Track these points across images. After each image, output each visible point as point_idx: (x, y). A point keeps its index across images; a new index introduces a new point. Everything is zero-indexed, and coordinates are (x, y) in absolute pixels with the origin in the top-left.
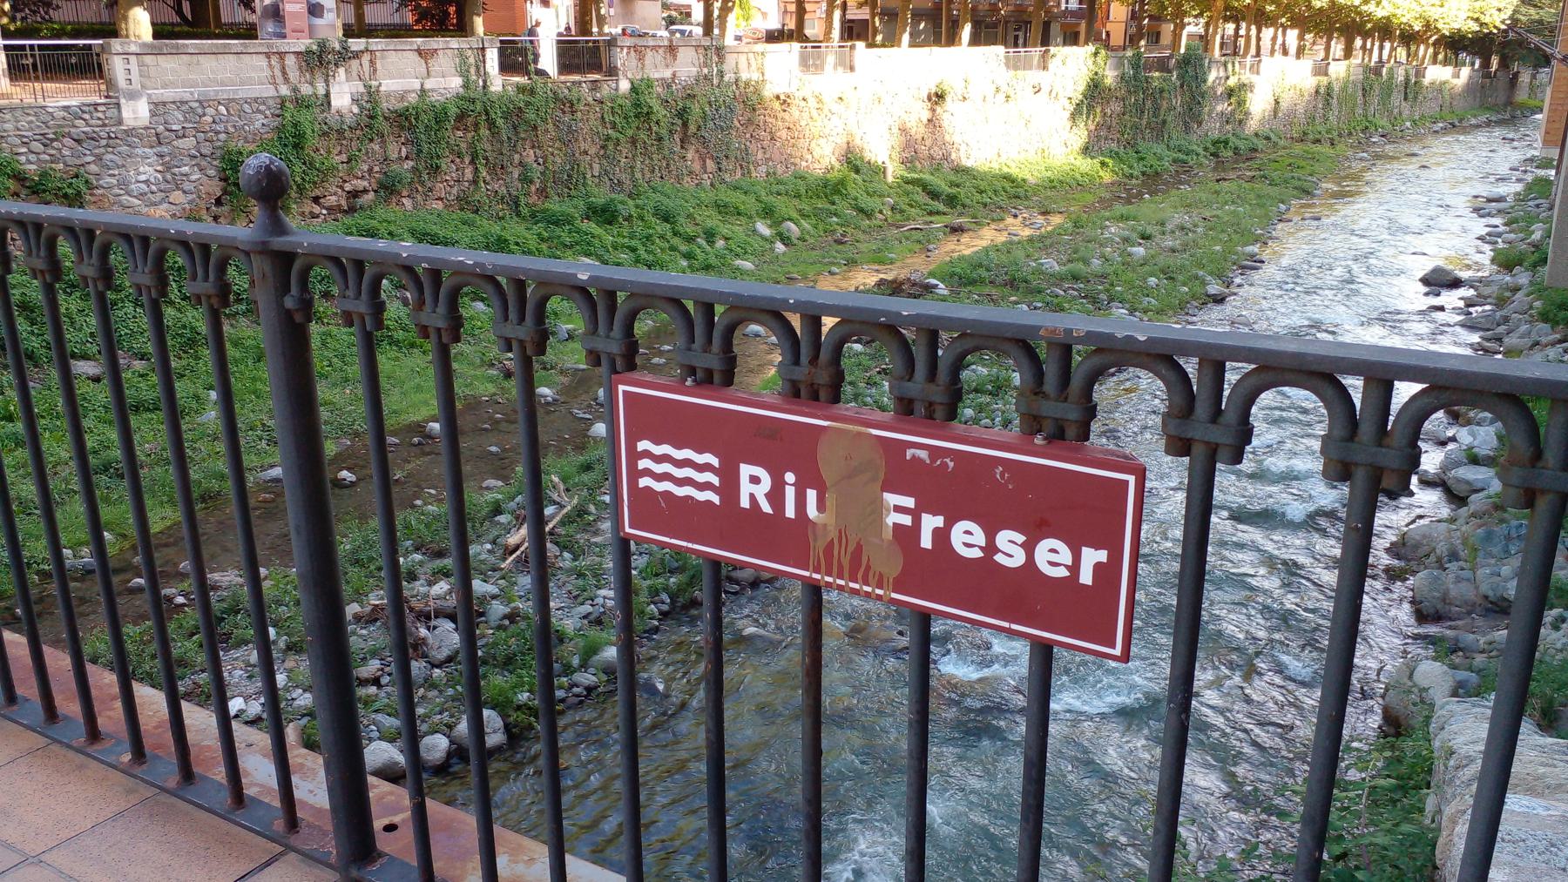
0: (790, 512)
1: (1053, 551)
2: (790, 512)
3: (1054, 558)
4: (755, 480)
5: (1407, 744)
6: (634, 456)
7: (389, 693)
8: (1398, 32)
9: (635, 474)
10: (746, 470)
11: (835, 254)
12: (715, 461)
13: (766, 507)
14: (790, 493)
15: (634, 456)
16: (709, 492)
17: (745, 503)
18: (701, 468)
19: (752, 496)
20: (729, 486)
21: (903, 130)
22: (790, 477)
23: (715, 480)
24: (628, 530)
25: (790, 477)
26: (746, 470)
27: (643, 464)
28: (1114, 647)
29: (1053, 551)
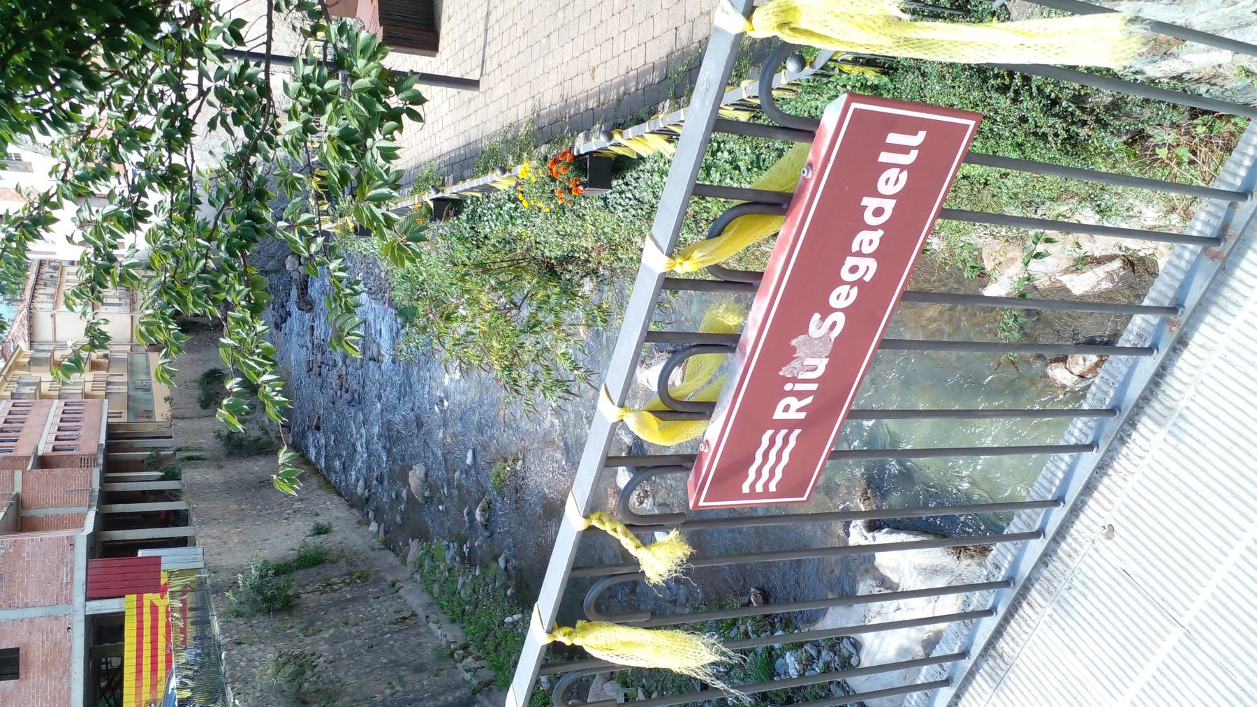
2: (814, 387)
4: (787, 408)
5: (88, 367)
7: (1175, 223)
10: (779, 414)
11: (474, 331)
12: (770, 432)
13: (809, 400)
15: (746, 497)
17: (802, 415)
18: (772, 442)
19: (799, 410)
20: (791, 425)
21: (7, 211)
23: (784, 432)
26: (779, 414)
27: (759, 489)
28: (119, 618)
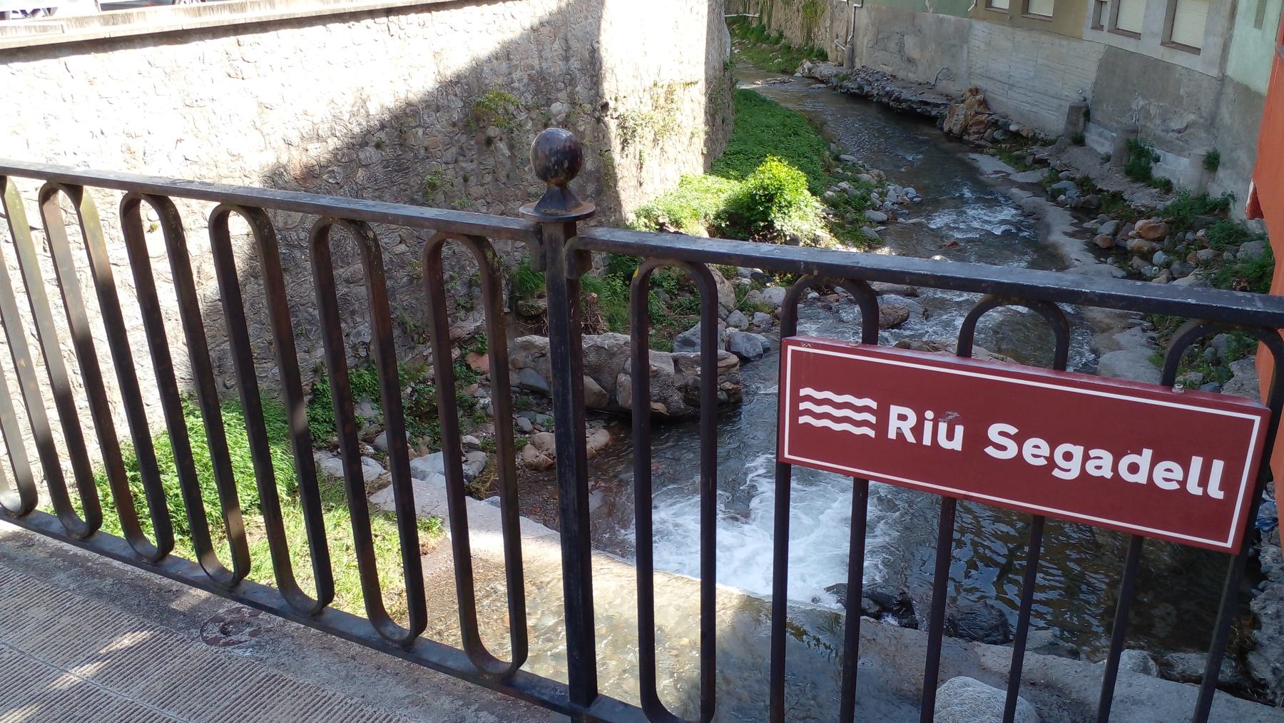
0: (927, 441)
1: (1169, 470)
2: (927, 441)
3: (1036, 451)
4: (902, 417)
6: (796, 399)
8: (273, 385)
9: (796, 413)
10: (895, 410)
12: (874, 405)
13: (910, 438)
14: (928, 426)
15: (796, 399)
16: (1212, 496)
17: (892, 435)
18: (859, 410)
20: (882, 426)
22: (929, 414)
23: (873, 419)
24: (787, 455)
25: (929, 414)
26: (895, 410)
27: (803, 406)
29: (1169, 470)
